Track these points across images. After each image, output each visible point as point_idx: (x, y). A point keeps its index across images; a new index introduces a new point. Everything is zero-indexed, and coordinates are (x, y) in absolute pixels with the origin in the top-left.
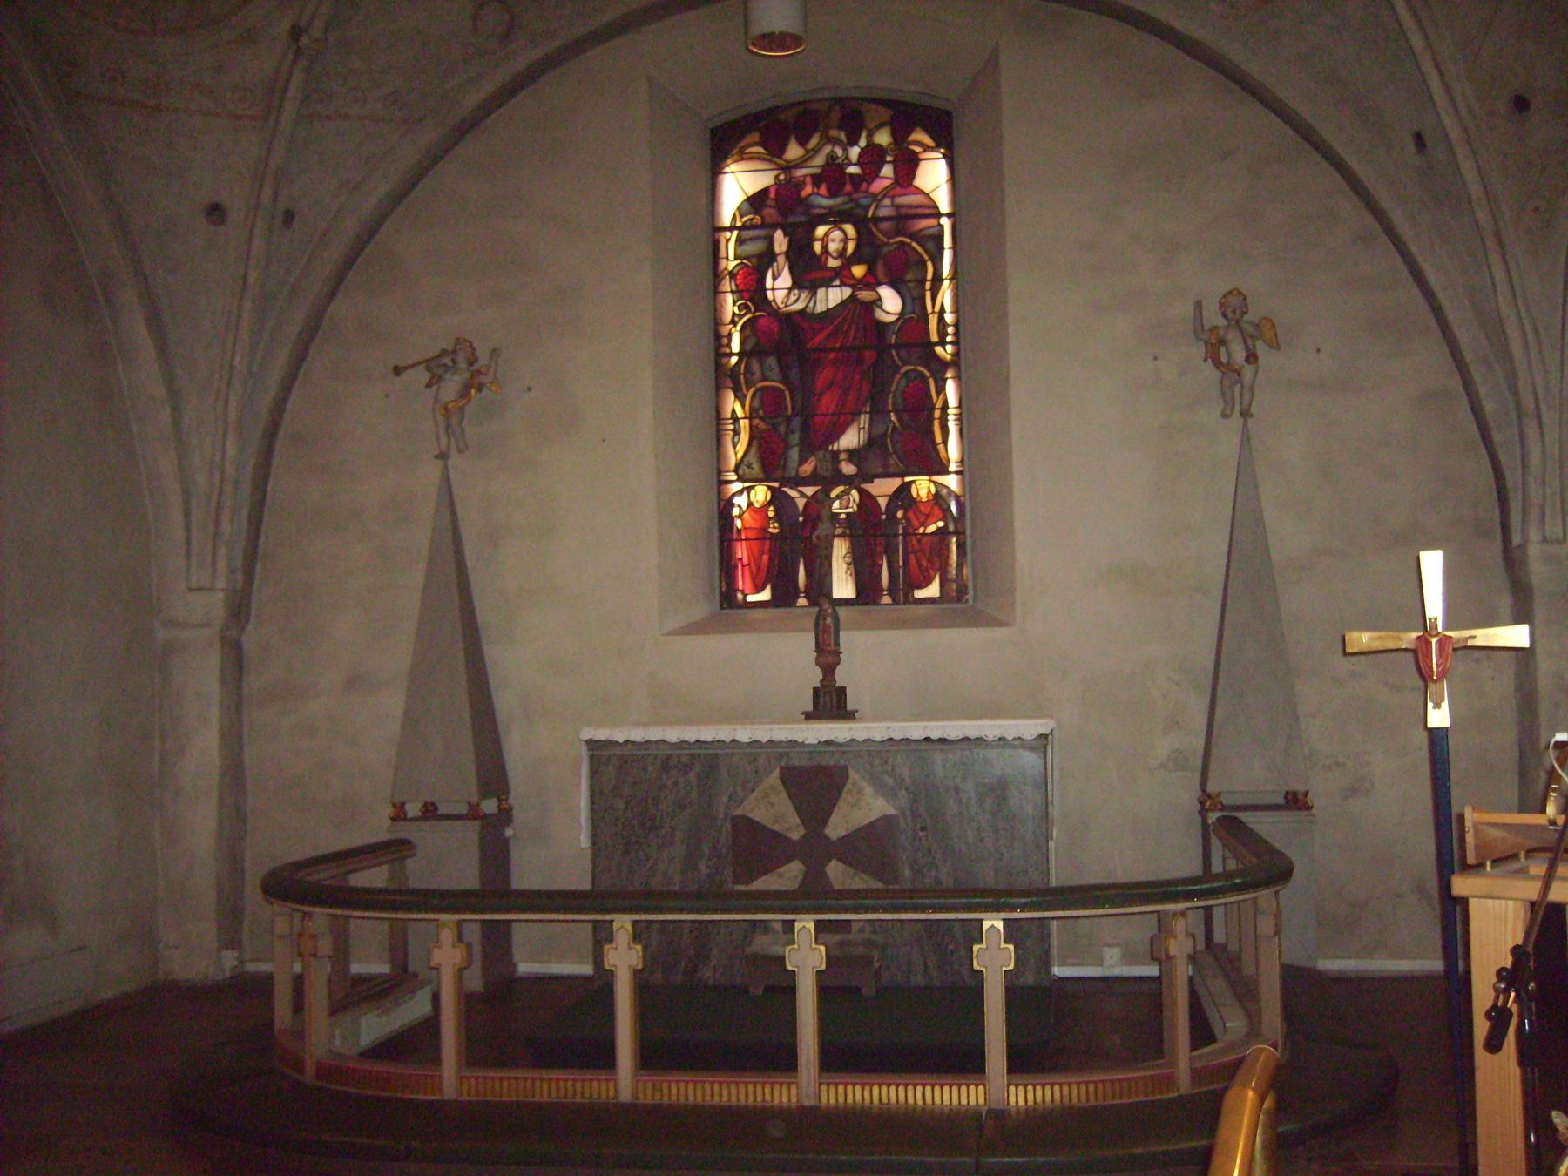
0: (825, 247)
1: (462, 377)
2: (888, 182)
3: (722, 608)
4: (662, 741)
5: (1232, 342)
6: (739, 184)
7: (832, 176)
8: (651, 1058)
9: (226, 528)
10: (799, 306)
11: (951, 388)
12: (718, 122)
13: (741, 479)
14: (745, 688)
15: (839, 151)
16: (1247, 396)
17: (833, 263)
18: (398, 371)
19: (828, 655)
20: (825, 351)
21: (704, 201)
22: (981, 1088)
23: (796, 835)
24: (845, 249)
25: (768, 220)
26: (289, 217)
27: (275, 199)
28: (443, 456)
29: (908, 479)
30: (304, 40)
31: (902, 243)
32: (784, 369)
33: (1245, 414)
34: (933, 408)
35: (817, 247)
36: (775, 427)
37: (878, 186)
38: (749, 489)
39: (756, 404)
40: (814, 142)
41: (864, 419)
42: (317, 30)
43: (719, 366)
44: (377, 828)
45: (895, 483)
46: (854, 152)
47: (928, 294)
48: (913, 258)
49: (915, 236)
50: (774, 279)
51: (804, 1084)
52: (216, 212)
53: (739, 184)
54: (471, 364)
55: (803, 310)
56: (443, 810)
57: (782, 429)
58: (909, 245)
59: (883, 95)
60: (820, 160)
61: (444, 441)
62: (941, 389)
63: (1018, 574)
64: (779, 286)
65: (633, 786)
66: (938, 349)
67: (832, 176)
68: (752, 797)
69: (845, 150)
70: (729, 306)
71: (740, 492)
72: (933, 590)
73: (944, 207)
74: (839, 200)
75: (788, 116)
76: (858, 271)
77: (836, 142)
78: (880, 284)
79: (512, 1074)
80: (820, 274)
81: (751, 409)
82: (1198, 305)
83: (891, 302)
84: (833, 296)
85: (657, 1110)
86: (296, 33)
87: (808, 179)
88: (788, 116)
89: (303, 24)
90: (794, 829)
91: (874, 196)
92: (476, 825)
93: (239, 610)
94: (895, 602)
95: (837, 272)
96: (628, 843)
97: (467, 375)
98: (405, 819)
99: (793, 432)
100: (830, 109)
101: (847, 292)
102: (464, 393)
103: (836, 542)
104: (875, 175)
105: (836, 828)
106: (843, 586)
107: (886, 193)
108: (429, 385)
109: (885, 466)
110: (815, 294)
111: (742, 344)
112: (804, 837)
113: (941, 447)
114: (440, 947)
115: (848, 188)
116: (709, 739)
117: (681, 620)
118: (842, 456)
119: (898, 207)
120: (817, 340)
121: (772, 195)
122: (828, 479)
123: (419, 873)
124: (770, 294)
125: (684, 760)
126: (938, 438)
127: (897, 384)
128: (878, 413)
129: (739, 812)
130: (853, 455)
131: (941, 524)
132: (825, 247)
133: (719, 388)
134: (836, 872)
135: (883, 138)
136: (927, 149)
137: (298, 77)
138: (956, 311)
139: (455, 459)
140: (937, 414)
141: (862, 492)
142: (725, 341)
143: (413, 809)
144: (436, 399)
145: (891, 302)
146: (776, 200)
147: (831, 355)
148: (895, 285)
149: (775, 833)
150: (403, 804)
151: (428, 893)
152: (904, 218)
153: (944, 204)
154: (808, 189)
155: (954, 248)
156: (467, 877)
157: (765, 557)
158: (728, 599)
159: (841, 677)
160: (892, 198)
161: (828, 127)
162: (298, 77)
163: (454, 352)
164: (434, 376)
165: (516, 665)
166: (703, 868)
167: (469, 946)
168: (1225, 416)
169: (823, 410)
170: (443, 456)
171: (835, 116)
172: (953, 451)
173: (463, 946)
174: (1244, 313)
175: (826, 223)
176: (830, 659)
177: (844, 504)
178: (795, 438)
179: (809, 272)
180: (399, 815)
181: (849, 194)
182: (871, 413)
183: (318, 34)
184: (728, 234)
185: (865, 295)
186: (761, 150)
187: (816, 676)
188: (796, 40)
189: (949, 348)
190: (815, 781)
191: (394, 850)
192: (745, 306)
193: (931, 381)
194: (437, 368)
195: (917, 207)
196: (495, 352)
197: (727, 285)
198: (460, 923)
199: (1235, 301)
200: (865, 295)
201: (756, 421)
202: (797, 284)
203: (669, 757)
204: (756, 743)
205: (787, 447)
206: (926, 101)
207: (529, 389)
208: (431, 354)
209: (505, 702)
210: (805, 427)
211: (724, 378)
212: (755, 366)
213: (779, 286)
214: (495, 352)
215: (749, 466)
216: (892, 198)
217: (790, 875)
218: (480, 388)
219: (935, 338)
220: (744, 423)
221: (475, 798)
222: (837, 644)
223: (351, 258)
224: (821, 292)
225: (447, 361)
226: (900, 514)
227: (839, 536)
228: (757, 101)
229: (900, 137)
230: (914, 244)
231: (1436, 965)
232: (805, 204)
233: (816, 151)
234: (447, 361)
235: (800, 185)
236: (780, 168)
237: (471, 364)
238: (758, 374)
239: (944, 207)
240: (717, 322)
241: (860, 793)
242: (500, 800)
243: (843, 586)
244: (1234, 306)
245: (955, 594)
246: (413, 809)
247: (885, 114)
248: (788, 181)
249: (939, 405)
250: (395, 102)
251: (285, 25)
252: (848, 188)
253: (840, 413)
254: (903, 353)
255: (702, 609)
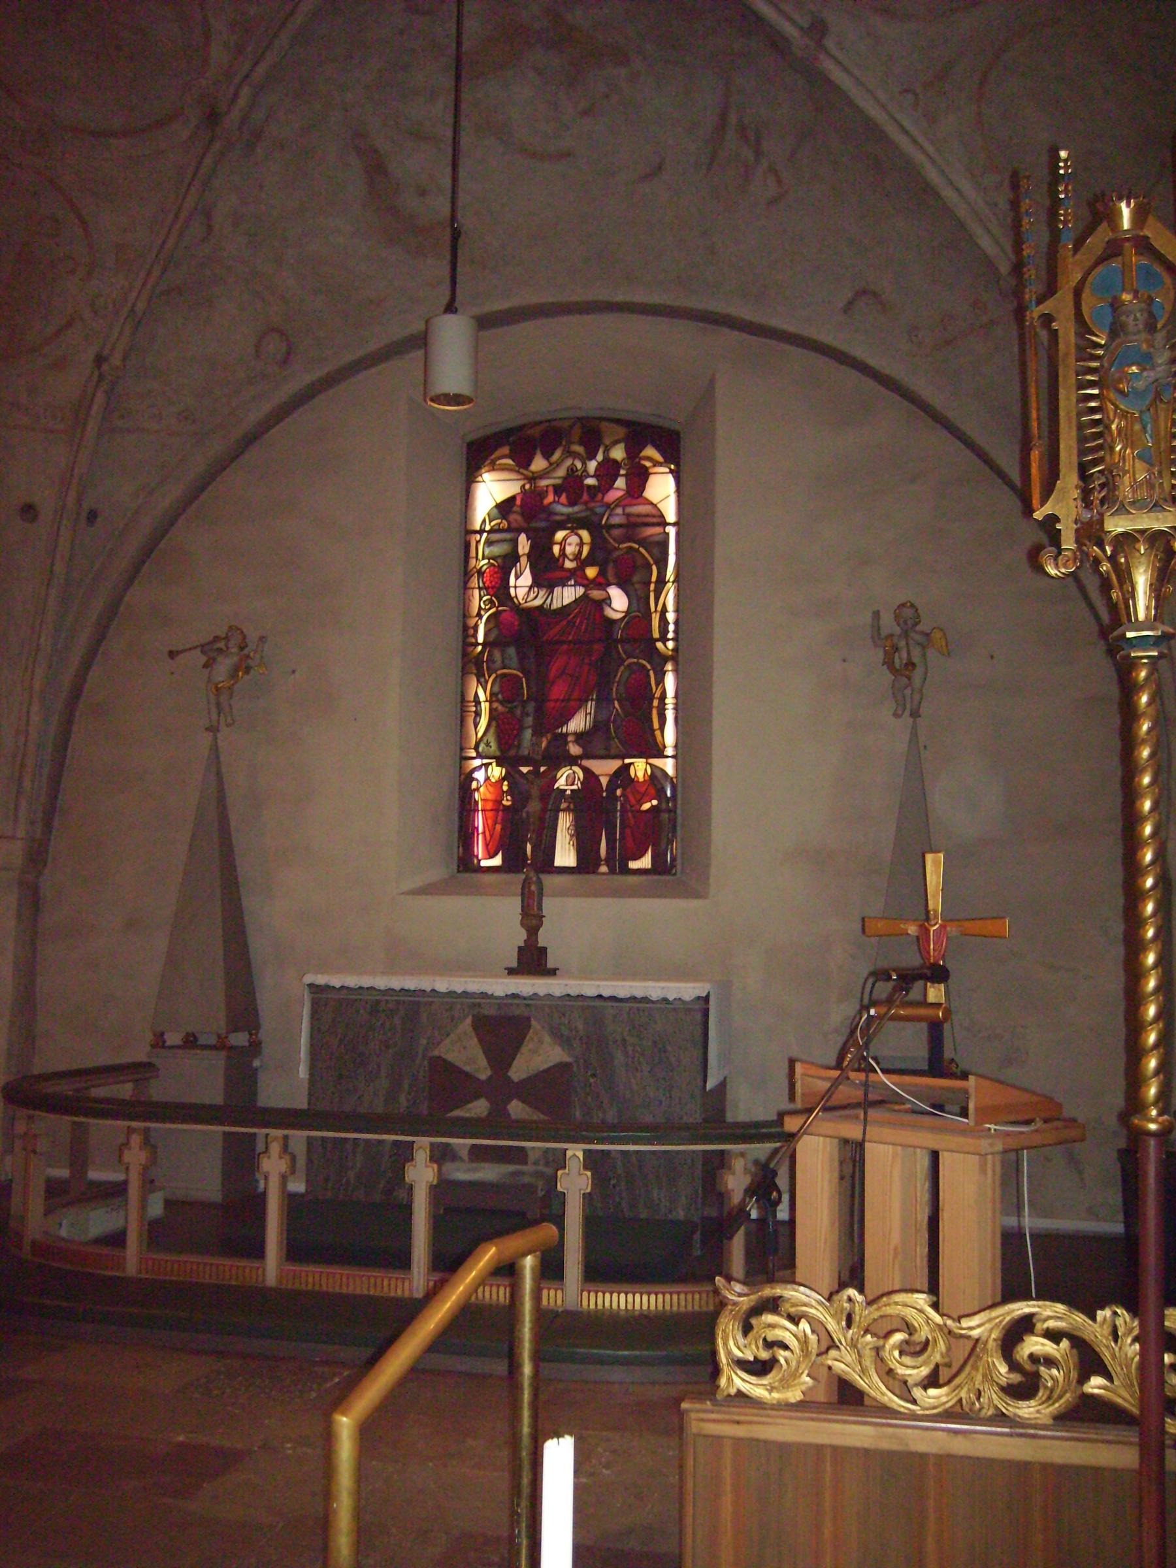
0: (563, 550)
1: (234, 657)
2: (620, 493)
3: (459, 871)
4: (372, 988)
5: (904, 649)
6: (492, 490)
7: (572, 486)
8: (295, 1252)
9: (27, 783)
10: (538, 602)
11: (670, 681)
12: (470, 438)
13: (480, 756)
14: (456, 945)
15: (579, 465)
16: (917, 697)
17: (569, 565)
18: (172, 654)
19: (532, 919)
20: (559, 642)
21: (459, 505)
22: (559, 1293)
23: (483, 1076)
24: (580, 552)
25: (514, 525)
26: (92, 516)
27: (79, 502)
28: (213, 729)
29: (627, 761)
30: (105, 367)
31: (631, 548)
32: (522, 658)
33: (915, 714)
34: (652, 698)
35: (556, 549)
36: (511, 711)
37: (612, 496)
38: (487, 765)
39: (496, 689)
40: (557, 455)
41: (591, 706)
42: (116, 360)
43: (465, 654)
44: (140, 1053)
45: (613, 765)
46: (592, 466)
47: (652, 595)
48: (639, 562)
49: (643, 542)
50: (517, 578)
51: (415, 1283)
52: (29, 511)
53: (492, 490)
54: (242, 649)
55: (540, 608)
56: (202, 1040)
57: (518, 712)
58: (637, 551)
59: (623, 416)
60: (561, 472)
61: (214, 715)
62: (660, 681)
63: (713, 850)
64: (521, 584)
65: (353, 1026)
66: (659, 645)
67: (572, 486)
68: (448, 1040)
69: (584, 464)
70: (477, 600)
71: (480, 767)
72: (645, 862)
73: (671, 517)
74: (576, 508)
75: (536, 432)
76: (591, 572)
77: (575, 455)
78: (610, 585)
79: (213, 1261)
80: (558, 574)
81: (492, 694)
82: (876, 615)
83: (619, 601)
84: (568, 595)
85: (297, 1294)
86: (99, 360)
87: (551, 489)
88: (536, 432)
89: (106, 352)
90: (481, 1068)
91: (608, 506)
92: (223, 1054)
93: (37, 856)
94: (612, 871)
95: (572, 573)
96: (341, 1077)
97: (236, 659)
98: (163, 1047)
99: (528, 715)
100: (571, 427)
101: (580, 591)
102: (234, 675)
103: (561, 815)
104: (610, 487)
105: (519, 1071)
106: (565, 856)
107: (619, 502)
108: (205, 666)
109: (607, 748)
110: (552, 592)
111: (486, 635)
112: (490, 1078)
113: (658, 733)
114: (130, 1149)
115: (585, 497)
116: (412, 988)
117: (418, 882)
118: (570, 738)
119: (628, 515)
120: (552, 633)
121: (518, 502)
122: (558, 758)
123: (157, 1091)
124: (512, 591)
125: (390, 1005)
126: (656, 725)
127: (621, 673)
128: (604, 700)
129: (436, 1053)
130: (580, 737)
131: (655, 802)
132: (563, 550)
133: (465, 673)
134: (516, 1109)
135: (618, 453)
136: (656, 464)
137: (100, 398)
138: (677, 611)
139: (224, 730)
140: (656, 703)
141: (586, 771)
142: (471, 632)
143: (173, 1039)
144: (209, 680)
145: (619, 601)
146: (522, 506)
147: (565, 647)
148: (623, 585)
149: (467, 1074)
150: (162, 1034)
151: (166, 1105)
152: (633, 526)
153: (670, 513)
154: (550, 498)
155: (677, 554)
156: (212, 1093)
157: (498, 827)
158: (467, 863)
159: (544, 938)
160: (624, 507)
161: (571, 443)
162: (100, 398)
163: (227, 638)
164: (210, 659)
165: (274, 915)
166: (402, 1099)
167: (293, 1159)
168: (896, 715)
169: (554, 697)
170: (213, 729)
171: (577, 432)
172: (669, 736)
173: (288, 1157)
174: (917, 624)
175: (565, 528)
176: (534, 922)
177: (566, 779)
178: (529, 721)
179: (548, 573)
180: (159, 1042)
181: (586, 503)
182: (597, 701)
183: (118, 363)
184: (478, 537)
185: (596, 594)
186: (510, 462)
187: (521, 936)
188: (469, 400)
189: (670, 645)
190: (502, 1027)
191: (140, 1071)
192: (491, 601)
193: (652, 673)
194: (211, 650)
195: (647, 516)
196: (262, 639)
197: (474, 582)
198: (286, 1137)
199: (908, 612)
200: (596, 594)
201: (495, 705)
202: (537, 583)
203: (378, 1002)
204: (451, 994)
205: (521, 728)
206: (654, 421)
207: (294, 672)
208: (206, 641)
209: (259, 946)
210: (538, 710)
211: (471, 664)
212: (497, 655)
213: (521, 584)
214: (262, 639)
215: (488, 744)
216: (624, 507)
217: (479, 1108)
218: (248, 670)
219: (656, 635)
220: (485, 706)
221: (223, 1032)
222: (540, 908)
223: (147, 552)
224: (558, 590)
225: (222, 645)
226: (619, 792)
227: (564, 810)
228: (508, 418)
229: (633, 453)
230: (641, 549)
231: (1118, 1228)
232: (548, 511)
233: (558, 464)
234: (222, 645)
235: (542, 494)
236: (526, 478)
237: (242, 649)
238: (499, 663)
239: (671, 517)
240: (466, 615)
241: (541, 1042)
242: (251, 1034)
243: (565, 856)
244: (908, 617)
245: (660, 867)
246: (173, 1039)
247: (621, 431)
248: (532, 491)
249: (657, 695)
250: (186, 418)
251: (90, 354)
252: (585, 497)
253: (569, 700)
254: (627, 647)
255: (437, 873)
